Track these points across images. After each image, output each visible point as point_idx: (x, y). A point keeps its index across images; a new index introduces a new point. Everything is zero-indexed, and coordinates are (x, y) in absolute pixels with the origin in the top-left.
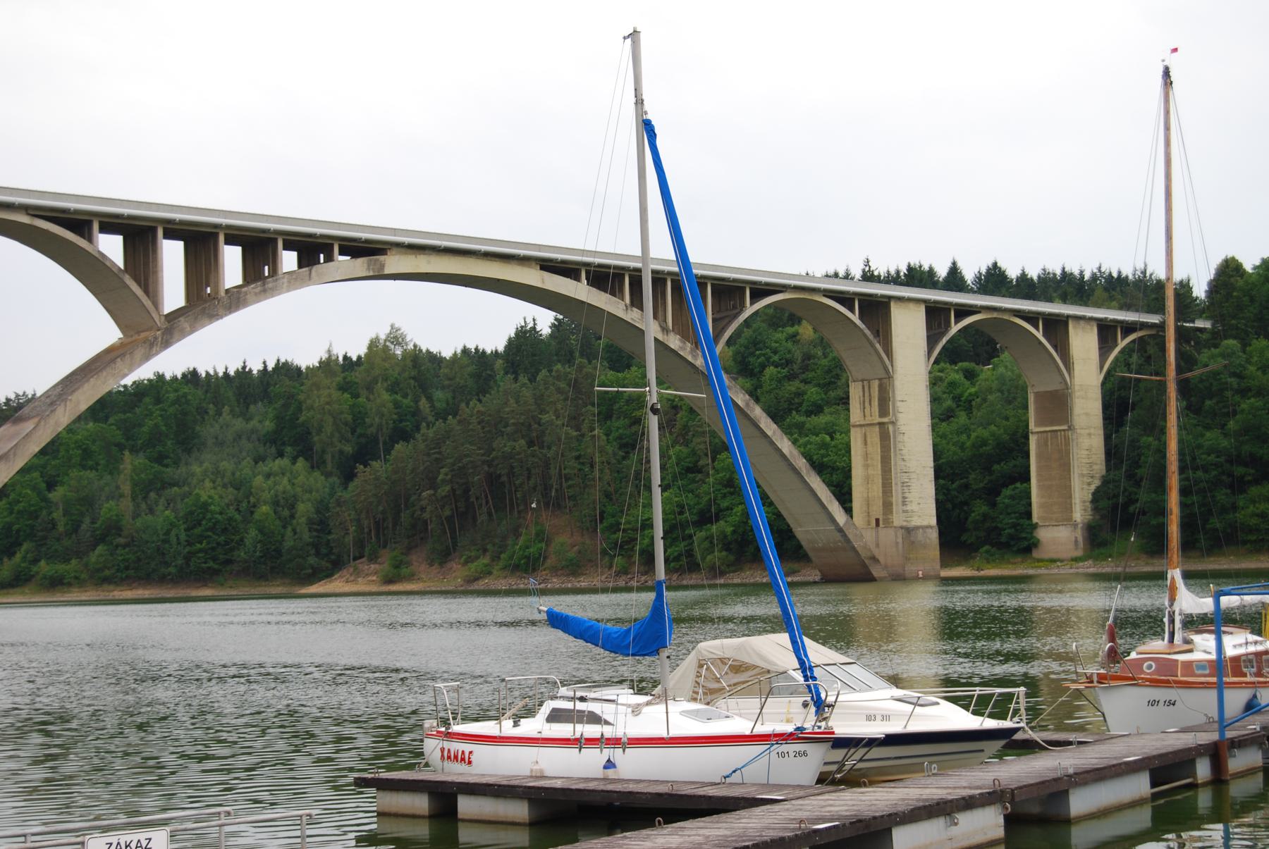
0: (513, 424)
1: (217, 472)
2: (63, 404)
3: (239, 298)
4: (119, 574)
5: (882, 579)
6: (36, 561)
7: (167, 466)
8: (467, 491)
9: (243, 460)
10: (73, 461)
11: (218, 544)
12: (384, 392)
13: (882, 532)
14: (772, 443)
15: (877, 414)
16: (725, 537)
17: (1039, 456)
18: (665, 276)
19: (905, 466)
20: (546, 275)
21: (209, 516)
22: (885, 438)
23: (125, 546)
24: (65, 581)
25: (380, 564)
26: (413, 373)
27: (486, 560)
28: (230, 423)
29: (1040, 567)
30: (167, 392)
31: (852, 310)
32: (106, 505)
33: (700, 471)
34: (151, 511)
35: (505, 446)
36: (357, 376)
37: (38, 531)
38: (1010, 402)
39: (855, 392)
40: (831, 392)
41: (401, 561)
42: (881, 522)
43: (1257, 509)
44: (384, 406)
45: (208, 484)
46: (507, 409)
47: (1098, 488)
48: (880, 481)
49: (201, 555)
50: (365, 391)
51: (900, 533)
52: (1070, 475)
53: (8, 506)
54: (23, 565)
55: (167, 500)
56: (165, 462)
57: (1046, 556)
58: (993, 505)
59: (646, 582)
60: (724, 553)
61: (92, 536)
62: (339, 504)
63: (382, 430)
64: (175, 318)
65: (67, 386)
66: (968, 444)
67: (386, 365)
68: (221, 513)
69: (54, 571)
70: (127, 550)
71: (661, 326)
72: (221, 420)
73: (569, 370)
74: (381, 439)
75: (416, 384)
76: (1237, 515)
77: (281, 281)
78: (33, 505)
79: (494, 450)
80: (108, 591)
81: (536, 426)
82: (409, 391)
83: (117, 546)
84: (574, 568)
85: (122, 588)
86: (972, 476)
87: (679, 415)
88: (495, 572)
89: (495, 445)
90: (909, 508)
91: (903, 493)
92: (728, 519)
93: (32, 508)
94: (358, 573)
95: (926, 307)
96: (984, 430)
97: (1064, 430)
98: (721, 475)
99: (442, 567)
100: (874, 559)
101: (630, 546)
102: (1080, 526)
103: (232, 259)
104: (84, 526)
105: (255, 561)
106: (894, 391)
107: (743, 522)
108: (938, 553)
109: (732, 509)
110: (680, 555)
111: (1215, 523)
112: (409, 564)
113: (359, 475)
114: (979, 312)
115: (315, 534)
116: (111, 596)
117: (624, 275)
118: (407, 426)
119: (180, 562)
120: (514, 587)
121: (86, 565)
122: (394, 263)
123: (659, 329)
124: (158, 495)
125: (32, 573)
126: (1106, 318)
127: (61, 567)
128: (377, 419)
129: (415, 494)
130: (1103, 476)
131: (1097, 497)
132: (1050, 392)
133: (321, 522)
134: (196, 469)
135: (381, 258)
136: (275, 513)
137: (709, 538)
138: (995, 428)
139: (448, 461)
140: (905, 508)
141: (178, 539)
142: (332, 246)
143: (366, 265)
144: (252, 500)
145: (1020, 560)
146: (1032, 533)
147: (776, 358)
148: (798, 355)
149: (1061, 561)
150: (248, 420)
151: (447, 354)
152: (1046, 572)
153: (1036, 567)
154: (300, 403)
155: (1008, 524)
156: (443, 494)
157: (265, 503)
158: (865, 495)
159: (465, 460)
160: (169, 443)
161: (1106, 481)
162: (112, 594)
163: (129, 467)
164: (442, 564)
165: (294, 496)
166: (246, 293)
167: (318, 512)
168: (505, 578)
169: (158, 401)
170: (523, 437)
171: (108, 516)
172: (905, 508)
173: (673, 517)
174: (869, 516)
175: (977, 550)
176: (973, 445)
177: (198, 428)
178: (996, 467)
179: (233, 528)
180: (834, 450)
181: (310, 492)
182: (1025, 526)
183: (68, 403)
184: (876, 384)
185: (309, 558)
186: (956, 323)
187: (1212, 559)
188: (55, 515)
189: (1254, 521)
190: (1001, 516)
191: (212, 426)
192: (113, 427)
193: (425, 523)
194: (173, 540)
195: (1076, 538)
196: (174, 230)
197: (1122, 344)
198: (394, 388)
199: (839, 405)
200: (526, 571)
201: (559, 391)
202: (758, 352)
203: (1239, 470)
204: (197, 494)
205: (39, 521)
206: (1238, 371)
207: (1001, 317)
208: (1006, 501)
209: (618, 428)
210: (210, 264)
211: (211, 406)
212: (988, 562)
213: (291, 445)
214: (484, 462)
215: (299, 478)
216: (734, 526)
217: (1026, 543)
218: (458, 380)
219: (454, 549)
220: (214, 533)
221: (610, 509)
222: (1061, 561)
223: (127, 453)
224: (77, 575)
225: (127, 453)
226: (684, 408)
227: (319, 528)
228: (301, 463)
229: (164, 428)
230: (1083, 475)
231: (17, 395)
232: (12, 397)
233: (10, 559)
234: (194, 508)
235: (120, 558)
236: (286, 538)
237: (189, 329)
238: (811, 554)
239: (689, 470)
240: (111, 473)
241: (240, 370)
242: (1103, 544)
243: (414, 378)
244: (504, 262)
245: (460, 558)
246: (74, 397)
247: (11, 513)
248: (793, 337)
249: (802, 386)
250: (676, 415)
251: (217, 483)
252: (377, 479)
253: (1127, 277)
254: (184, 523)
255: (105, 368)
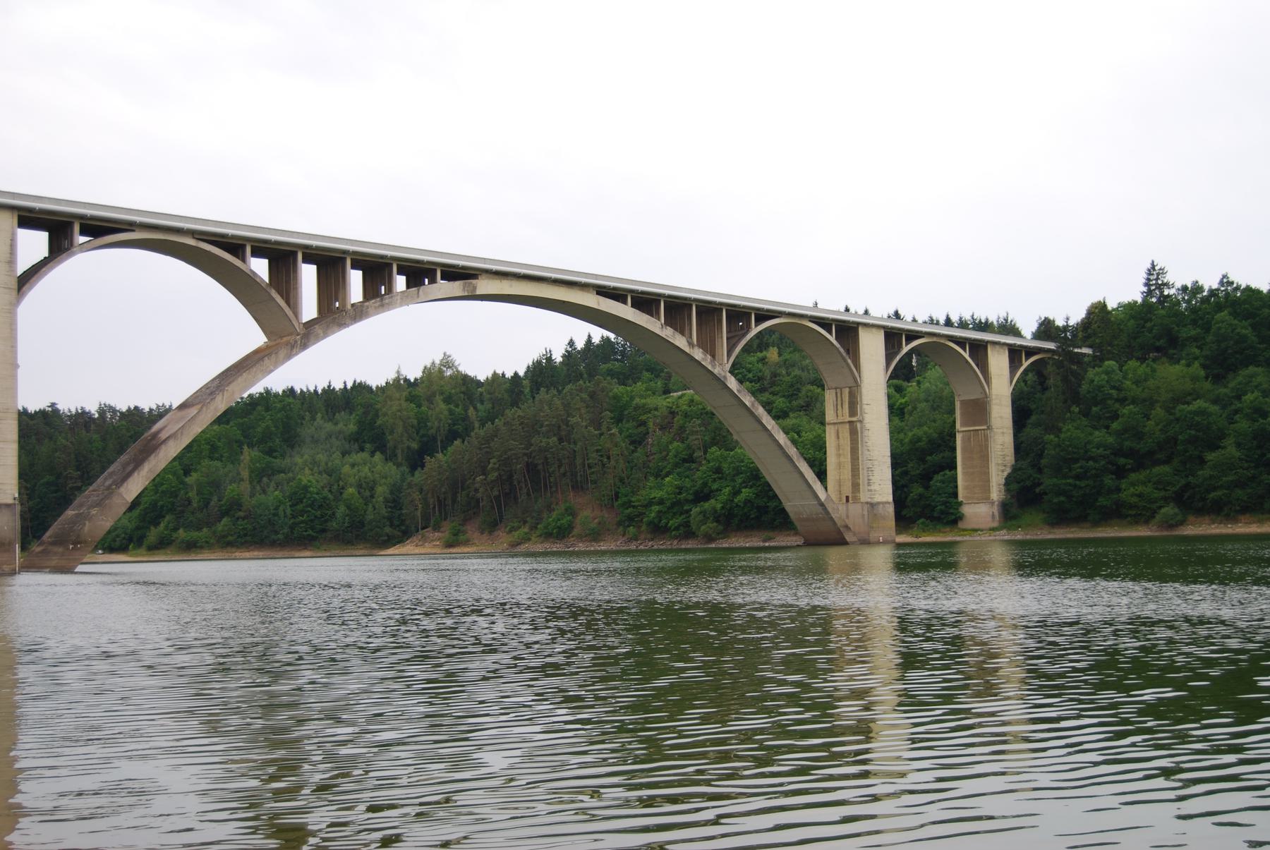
0: (547, 425)
1: (315, 463)
2: (221, 393)
3: (362, 311)
4: (240, 539)
5: (853, 543)
6: (176, 529)
7: (275, 458)
8: (511, 477)
9: (333, 453)
10: (204, 454)
11: (316, 517)
12: (442, 403)
13: (851, 506)
14: (771, 436)
15: (848, 414)
16: (716, 511)
17: (964, 450)
18: (692, 303)
19: (870, 455)
20: (602, 299)
21: (309, 495)
22: (854, 433)
23: (244, 519)
24: (198, 545)
25: (442, 532)
26: (463, 389)
27: (526, 530)
28: (321, 425)
29: (965, 535)
30: (274, 403)
31: (830, 332)
32: (229, 487)
33: (693, 462)
34: (264, 492)
35: (541, 442)
36: (420, 391)
37: (178, 506)
38: (934, 410)
39: (829, 397)
40: (794, 402)
41: (459, 530)
42: (850, 499)
43: (1137, 490)
44: (442, 413)
45: (307, 471)
46: (542, 414)
47: (1009, 474)
48: (850, 467)
49: (302, 525)
50: (426, 402)
51: (866, 507)
52: (988, 464)
53: (154, 488)
54: (165, 532)
55: (276, 484)
56: (275, 454)
57: (969, 527)
58: (927, 487)
59: (653, 546)
60: (715, 524)
61: (219, 511)
62: (410, 486)
63: (440, 431)
64: (311, 326)
65: (223, 379)
66: (907, 440)
67: (442, 382)
68: (317, 494)
69: (189, 537)
70: (246, 521)
71: (688, 342)
72: (315, 423)
73: (589, 384)
74: (439, 438)
75: (466, 397)
76: (1120, 495)
77: (395, 298)
78: (173, 487)
79: (532, 445)
80: (231, 553)
81: (565, 427)
82: (460, 403)
83: (238, 519)
84: (595, 536)
85: (242, 550)
86: (911, 465)
87: (675, 419)
88: (533, 538)
89: (533, 441)
90: (872, 488)
91: (868, 476)
92: (718, 498)
93: (173, 489)
94: (425, 539)
95: (885, 332)
96: (918, 431)
97: (984, 430)
98: (711, 464)
99: (491, 534)
100: (847, 527)
101: (639, 519)
102: (996, 503)
103: (355, 278)
104: (212, 503)
105: (343, 530)
106: (861, 397)
107: (730, 500)
108: (894, 523)
109: (721, 490)
110: (679, 526)
111: (1102, 501)
112: (465, 532)
113: (426, 464)
114: (923, 337)
115: (389, 510)
116: (302, 555)
117: (660, 301)
118: (459, 428)
119: (286, 530)
120: (549, 550)
121: (214, 533)
122: (485, 286)
123: (687, 344)
124: (269, 479)
125: (173, 538)
126: (1015, 344)
127: (195, 535)
128: (436, 423)
129: (470, 479)
130: (1013, 466)
131: (1008, 481)
132: (972, 400)
133: (394, 501)
134: (299, 460)
135: (474, 281)
136: (359, 493)
137: (703, 513)
138: (927, 429)
139: (496, 453)
140: (869, 488)
141: (285, 513)
142: (435, 271)
143: (462, 287)
144: (341, 483)
145: (948, 529)
146: (957, 509)
147: (750, 375)
148: (767, 373)
149: (982, 530)
150: (336, 424)
151: (482, 377)
152: (971, 539)
153: (962, 535)
154: (377, 411)
155: (939, 501)
156: (493, 479)
157: (351, 486)
158: (838, 478)
159: (509, 453)
160: (277, 440)
161: (1015, 469)
162: (234, 555)
163: (248, 458)
164: (491, 533)
165: (373, 481)
166: (368, 307)
167: (392, 493)
168: (542, 543)
169: (267, 409)
170: (555, 435)
171: (231, 495)
172: (869, 488)
173: (674, 496)
174: (840, 494)
175: (914, 522)
176: (911, 442)
177: (299, 430)
178: (929, 458)
179: (327, 505)
180: (802, 445)
181: (386, 478)
182: (953, 504)
183: (225, 392)
184: (846, 391)
185: (385, 528)
186: (907, 345)
187: (1100, 529)
188: (190, 494)
189: (1134, 500)
190: (934, 496)
191: (309, 428)
192: (235, 428)
193: (478, 501)
194: (281, 513)
195: (993, 512)
196: (316, 255)
197: (1026, 364)
198: (448, 400)
199: (800, 411)
200: (557, 538)
201: (582, 400)
202: (736, 371)
203: (1122, 461)
204: (299, 479)
205: (179, 498)
206: (1117, 385)
207: (938, 341)
208: (938, 484)
209: (628, 429)
210: (339, 281)
211: (307, 413)
212: (924, 531)
213: (368, 443)
214: (525, 454)
215: (377, 467)
216: (722, 503)
217: (953, 517)
218: (497, 394)
219: (501, 521)
220: (312, 508)
221: (623, 490)
222: (982, 530)
223: (245, 447)
224: (208, 540)
225: (245, 447)
226: (680, 413)
227: (393, 505)
228: (378, 456)
229: (273, 429)
230: (998, 464)
231: (158, 406)
232: (154, 407)
233: (156, 528)
234: (297, 490)
235: (240, 527)
236: (367, 513)
237: (322, 335)
238: (796, 523)
239: (685, 461)
240: (232, 463)
241: (326, 388)
242: (1014, 517)
243: (463, 393)
244: (569, 288)
245: (506, 527)
246: (230, 388)
247: (156, 493)
248: (763, 360)
249: (771, 396)
250: (673, 418)
251: (314, 471)
252: (440, 467)
253: (992, 323)
254: (289, 501)
255: (255, 365)
